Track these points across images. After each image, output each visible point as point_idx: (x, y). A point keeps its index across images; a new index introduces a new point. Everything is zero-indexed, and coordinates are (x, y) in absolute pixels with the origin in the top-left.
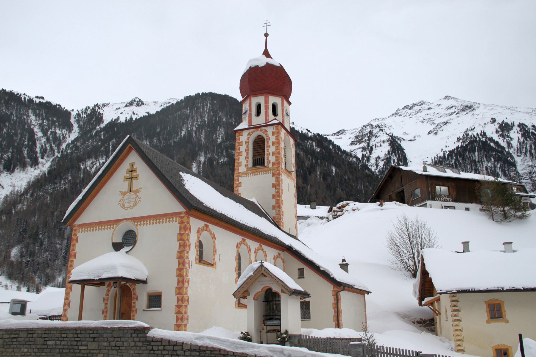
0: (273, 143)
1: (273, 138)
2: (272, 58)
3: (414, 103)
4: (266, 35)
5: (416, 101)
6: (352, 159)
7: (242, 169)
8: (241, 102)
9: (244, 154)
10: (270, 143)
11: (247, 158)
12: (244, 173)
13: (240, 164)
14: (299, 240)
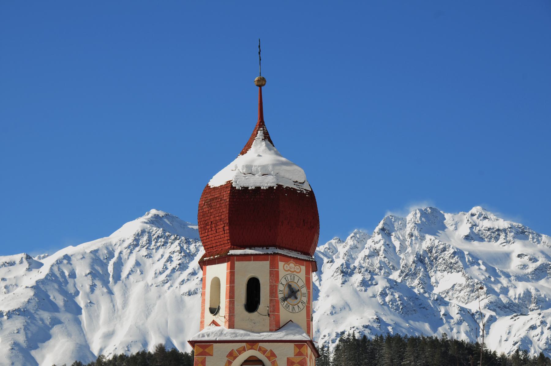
4: (261, 83)
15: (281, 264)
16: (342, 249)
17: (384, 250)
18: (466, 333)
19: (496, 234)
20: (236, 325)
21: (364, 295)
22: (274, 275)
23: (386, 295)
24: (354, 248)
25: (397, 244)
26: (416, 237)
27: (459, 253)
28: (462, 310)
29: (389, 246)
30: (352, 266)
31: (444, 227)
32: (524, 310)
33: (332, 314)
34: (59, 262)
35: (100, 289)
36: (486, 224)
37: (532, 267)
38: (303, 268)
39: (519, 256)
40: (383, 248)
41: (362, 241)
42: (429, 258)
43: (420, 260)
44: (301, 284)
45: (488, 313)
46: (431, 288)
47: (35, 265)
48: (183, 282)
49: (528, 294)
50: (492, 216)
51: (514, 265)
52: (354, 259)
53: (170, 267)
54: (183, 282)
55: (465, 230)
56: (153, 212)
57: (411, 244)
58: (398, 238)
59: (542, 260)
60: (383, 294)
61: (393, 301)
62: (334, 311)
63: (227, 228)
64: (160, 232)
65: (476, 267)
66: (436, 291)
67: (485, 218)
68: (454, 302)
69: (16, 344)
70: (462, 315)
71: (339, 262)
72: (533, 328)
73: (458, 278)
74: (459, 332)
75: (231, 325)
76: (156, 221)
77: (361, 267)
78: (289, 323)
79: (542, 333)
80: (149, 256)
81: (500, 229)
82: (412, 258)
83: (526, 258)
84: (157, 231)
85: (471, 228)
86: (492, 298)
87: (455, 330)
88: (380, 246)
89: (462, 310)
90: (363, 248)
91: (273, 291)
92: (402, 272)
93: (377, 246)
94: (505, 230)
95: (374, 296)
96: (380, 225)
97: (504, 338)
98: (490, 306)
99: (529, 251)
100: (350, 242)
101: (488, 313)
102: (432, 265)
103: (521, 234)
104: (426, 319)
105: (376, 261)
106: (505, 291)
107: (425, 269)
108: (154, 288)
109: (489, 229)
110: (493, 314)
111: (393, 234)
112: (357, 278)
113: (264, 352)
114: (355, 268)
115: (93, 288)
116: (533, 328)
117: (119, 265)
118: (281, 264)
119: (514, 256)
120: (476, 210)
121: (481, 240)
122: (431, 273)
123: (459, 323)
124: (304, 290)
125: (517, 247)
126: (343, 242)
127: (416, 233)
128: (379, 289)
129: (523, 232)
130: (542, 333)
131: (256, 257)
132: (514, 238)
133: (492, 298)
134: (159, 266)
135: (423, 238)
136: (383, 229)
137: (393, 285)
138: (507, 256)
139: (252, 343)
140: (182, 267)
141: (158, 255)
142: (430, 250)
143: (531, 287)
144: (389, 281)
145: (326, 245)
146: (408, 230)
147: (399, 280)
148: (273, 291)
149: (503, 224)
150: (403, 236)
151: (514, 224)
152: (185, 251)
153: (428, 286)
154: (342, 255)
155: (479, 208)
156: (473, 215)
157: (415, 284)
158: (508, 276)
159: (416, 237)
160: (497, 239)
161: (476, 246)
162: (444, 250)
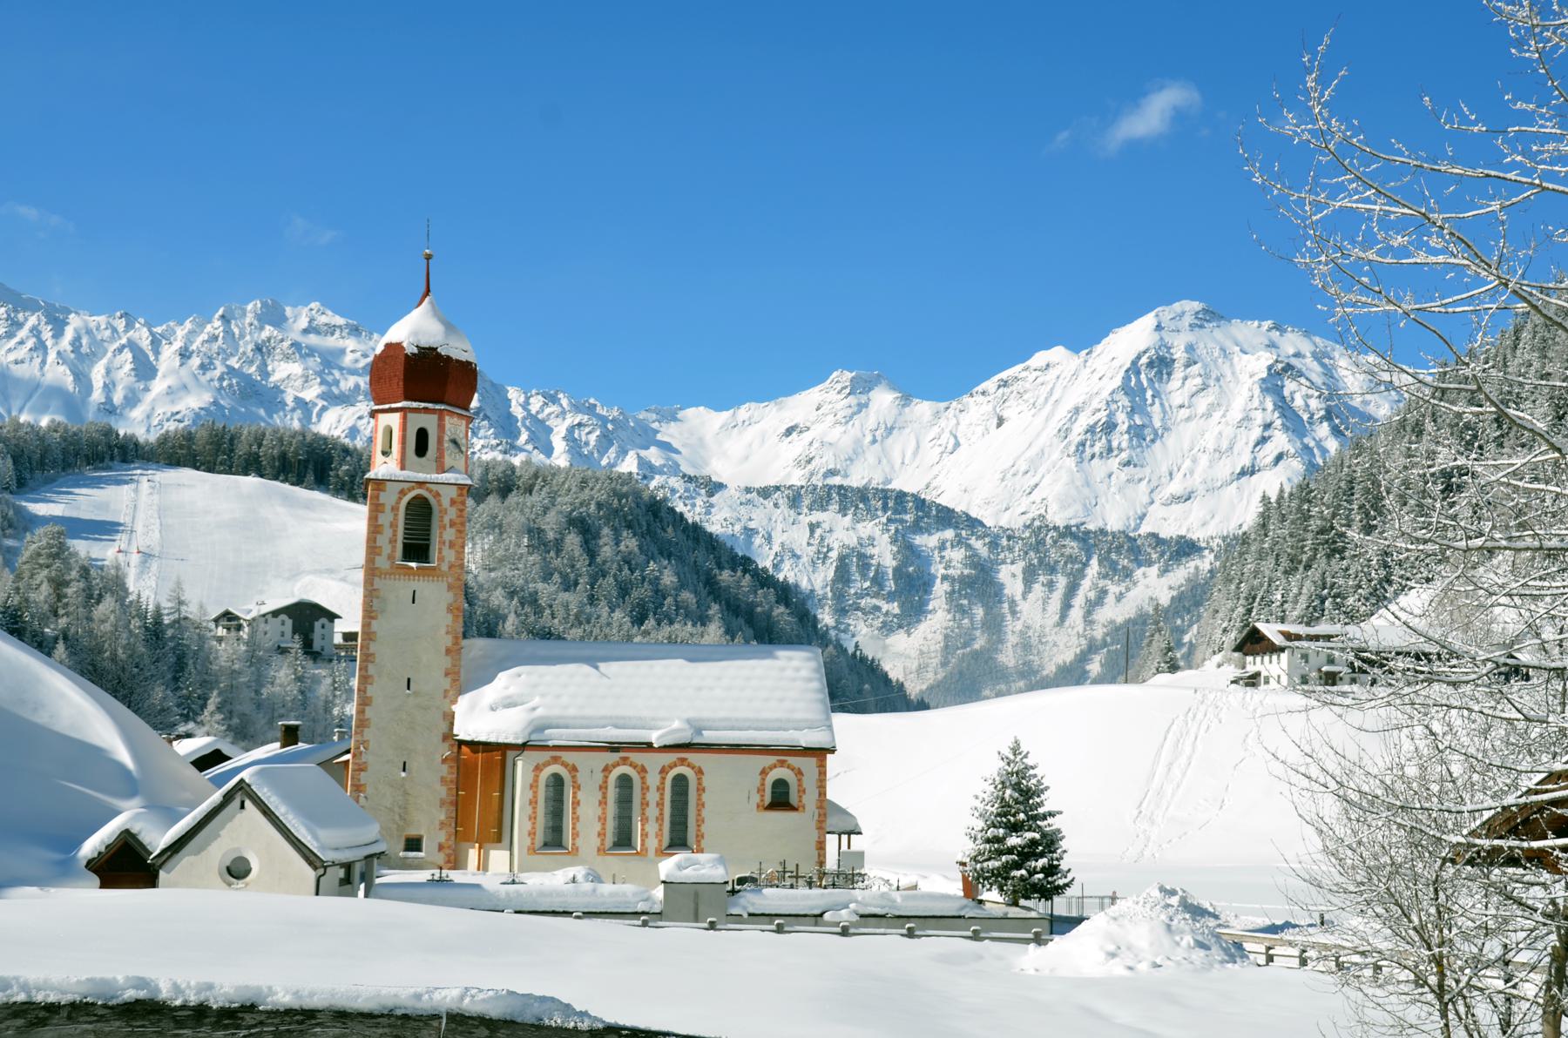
4: (428, 257)
10: (446, 520)
15: (447, 418)
16: (180, 332)
17: (223, 337)
18: (300, 420)
19: (331, 329)
20: (407, 467)
21: (203, 379)
22: (441, 427)
23: (224, 379)
24: (191, 332)
25: (236, 331)
26: (256, 327)
27: (295, 345)
28: (297, 399)
29: (228, 332)
30: (191, 349)
31: (285, 319)
32: (352, 400)
33: (167, 394)
36: (323, 319)
38: (464, 422)
39: (352, 351)
40: (221, 335)
41: (202, 326)
42: (267, 347)
43: (258, 349)
44: (462, 435)
45: (321, 403)
48: (10, 350)
50: (330, 313)
51: (348, 360)
52: (192, 343)
54: (10, 350)
55: (303, 323)
57: (250, 333)
58: (237, 326)
60: (221, 379)
61: (230, 386)
62: (170, 392)
63: (401, 383)
65: (312, 359)
66: (272, 379)
67: (323, 313)
68: (289, 390)
70: (296, 403)
71: (178, 345)
72: (360, 418)
73: (296, 368)
74: (292, 419)
75: (403, 468)
77: (199, 352)
78: (451, 469)
79: (369, 423)
81: (1109, 528)
82: (251, 347)
83: (359, 353)
85: (310, 322)
86: (324, 388)
87: (289, 417)
88: (220, 332)
89: (297, 399)
90: (202, 332)
91: (440, 441)
92: (240, 359)
93: (217, 332)
94: (340, 327)
95: (212, 380)
96: (221, 312)
97: (334, 426)
98: (322, 396)
99: (362, 347)
100: (188, 325)
101: (321, 403)
102: (269, 354)
103: (355, 331)
104: (261, 404)
105: (215, 347)
106: (337, 383)
107: (263, 357)
109: (326, 324)
110: (325, 403)
111: (233, 322)
112: (195, 362)
113: (430, 491)
114: (193, 352)
116: (360, 418)
118: (447, 418)
119: (348, 350)
122: (269, 362)
123: (293, 410)
125: (350, 343)
126: (182, 325)
127: (256, 323)
128: (217, 373)
129: (357, 330)
130: (369, 423)
131: (426, 410)
132: (349, 334)
133: (324, 388)
135: (262, 328)
136: (223, 317)
138: (343, 352)
139: (421, 484)
142: (269, 339)
144: (228, 366)
145: (164, 327)
146: (248, 320)
147: (237, 366)
148: (440, 441)
149: (340, 321)
150: (243, 324)
151: (350, 321)
152: (12, 319)
153: (266, 374)
154: (179, 338)
155: (318, 303)
156: (311, 310)
158: (341, 369)
159: (256, 327)
160: (332, 334)
161: (313, 339)
162: (282, 340)
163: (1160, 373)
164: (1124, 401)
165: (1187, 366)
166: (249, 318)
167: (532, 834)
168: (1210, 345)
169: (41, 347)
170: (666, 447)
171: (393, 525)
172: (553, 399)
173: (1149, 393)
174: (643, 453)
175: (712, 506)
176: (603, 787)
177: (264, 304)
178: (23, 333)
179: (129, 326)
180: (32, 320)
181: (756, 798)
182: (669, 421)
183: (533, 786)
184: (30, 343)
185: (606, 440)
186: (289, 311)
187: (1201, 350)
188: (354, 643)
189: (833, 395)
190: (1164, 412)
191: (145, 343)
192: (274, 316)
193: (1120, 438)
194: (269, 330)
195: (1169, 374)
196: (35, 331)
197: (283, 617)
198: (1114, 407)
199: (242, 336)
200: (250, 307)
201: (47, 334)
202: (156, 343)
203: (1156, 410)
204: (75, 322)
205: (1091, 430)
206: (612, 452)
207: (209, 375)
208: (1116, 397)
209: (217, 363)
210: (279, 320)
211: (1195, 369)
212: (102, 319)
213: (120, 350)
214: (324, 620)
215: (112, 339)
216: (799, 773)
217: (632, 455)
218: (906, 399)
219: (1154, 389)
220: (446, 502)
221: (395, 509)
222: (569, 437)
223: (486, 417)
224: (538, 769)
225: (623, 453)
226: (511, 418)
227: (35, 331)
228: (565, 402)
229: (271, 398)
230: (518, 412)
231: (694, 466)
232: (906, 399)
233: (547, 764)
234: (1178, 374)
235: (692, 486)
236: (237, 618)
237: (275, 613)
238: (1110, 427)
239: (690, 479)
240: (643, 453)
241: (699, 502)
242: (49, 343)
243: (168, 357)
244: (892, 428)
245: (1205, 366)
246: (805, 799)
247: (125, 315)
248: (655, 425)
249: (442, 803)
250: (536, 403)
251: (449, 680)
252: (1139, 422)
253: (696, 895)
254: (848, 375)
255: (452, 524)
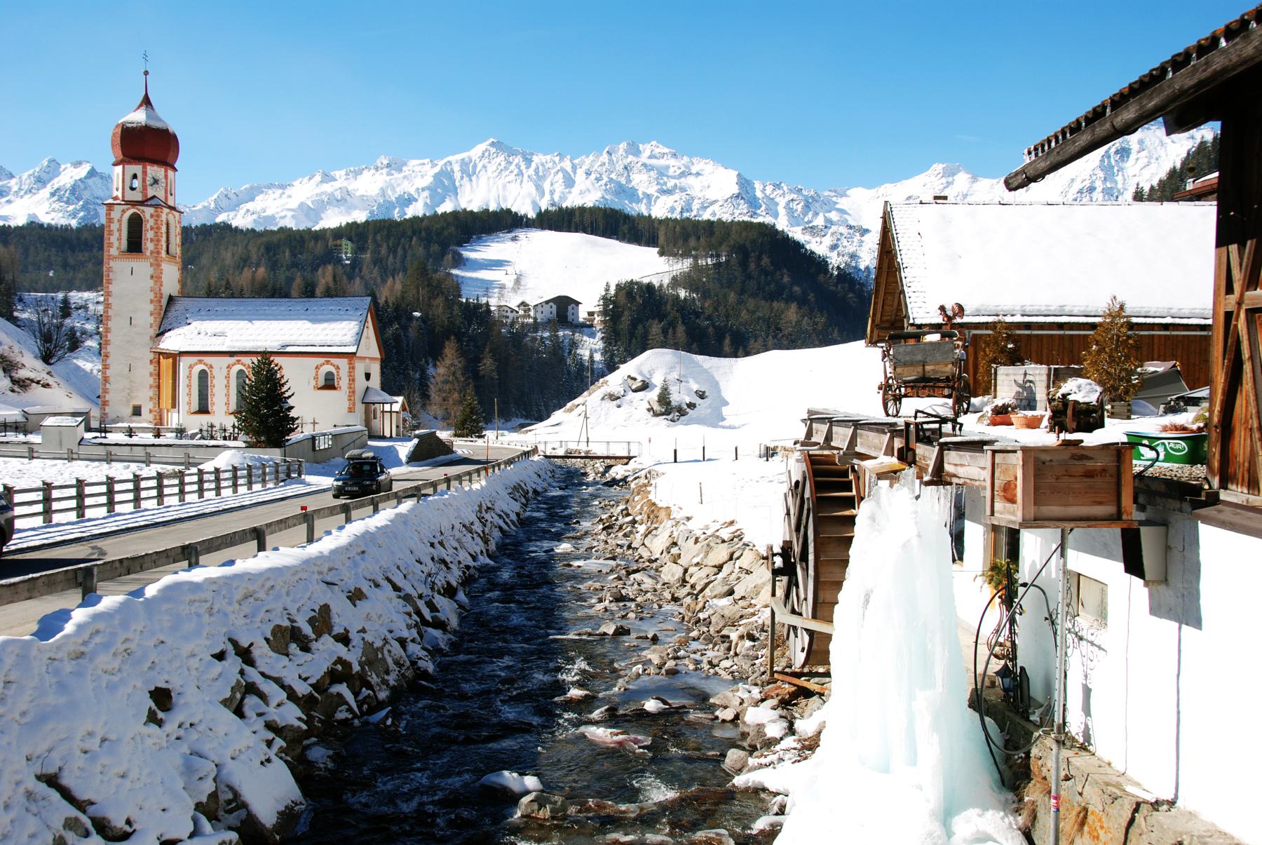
0: (152, 228)
1: (151, 222)
2: (195, 413)
3: (767, 785)
4: (146, 73)
5: (781, 790)
6: (703, 304)
7: (114, 251)
8: (279, 827)
9: (116, 234)
10: (148, 226)
11: (119, 239)
12: (115, 258)
13: (110, 245)
14: (146, 94)
21: (597, 185)
22: (145, 173)
25: (615, 159)
27: (644, 165)
28: (644, 193)
29: (611, 161)
34: (445, 164)
35: (466, 179)
36: (657, 151)
37: (678, 172)
41: (598, 157)
46: (631, 181)
47: (434, 165)
49: (676, 185)
51: (671, 172)
53: (500, 168)
55: (647, 153)
56: (492, 140)
59: (683, 169)
60: (606, 185)
64: (494, 150)
69: (426, 203)
71: (585, 167)
76: (493, 144)
80: (489, 162)
84: (493, 150)
86: (659, 187)
88: (606, 160)
98: (658, 191)
100: (591, 157)
103: (674, 155)
108: (492, 179)
115: (462, 178)
117: (475, 166)
120: (654, 143)
121: (656, 158)
124: (164, 180)
125: (672, 162)
128: (603, 182)
133: (659, 187)
134: (494, 168)
135: (627, 157)
137: (611, 180)
138: (668, 167)
140: (506, 168)
141: (493, 162)
143: (677, 181)
149: (666, 150)
153: (629, 180)
157: (623, 181)
158: (668, 176)
161: (653, 162)
163: (1122, 156)
164: (1101, 174)
165: (1139, 152)
166: (621, 152)
167: (189, 403)
168: (1153, 139)
169: (521, 174)
170: (842, 211)
171: (119, 230)
172: (777, 186)
173: (1116, 169)
174: (827, 215)
175: (862, 242)
176: (228, 377)
177: (628, 144)
178: (512, 167)
179: (561, 160)
180: (516, 161)
181: (313, 383)
182: (842, 196)
183: (189, 377)
184: (516, 171)
185: (807, 207)
186: (641, 147)
187: (1147, 143)
188: (1156, 341)
189: (933, 178)
190: (1125, 180)
191: (569, 169)
192: (634, 150)
193: (1098, 195)
194: (631, 158)
195: (1128, 157)
196: (518, 166)
197: (551, 304)
198: (1094, 178)
199: (617, 162)
200: (621, 146)
201: (523, 167)
202: (574, 168)
203: (1119, 179)
204: (536, 159)
205: (1080, 192)
206: (810, 215)
207: (600, 183)
208: (1096, 172)
209: (604, 176)
210: (637, 153)
211: (1144, 154)
212: (548, 157)
213: (557, 172)
214: (573, 305)
215: (553, 168)
216: (338, 368)
217: (821, 215)
218: (975, 179)
219: (1118, 166)
220: (148, 216)
221: (120, 221)
222: (787, 207)
223: (742, 198)
224: (191, 367)
225: (816, 214)
226: (755, 197)
227: (518, 166)
228: (785, 188)
229: (632, 194)
230: (759, 194)
231: (855, 221)
232: (975, 179)
233: (196, 364)
234: (1133, 156)
235: (851, 231)
236: (528, 305)
237: (547, 302)
238: (1091, 189)
239: (851, 227)
240: (827, 215)
241: (855, 240)
242: (524, 171)
243: (580, 177)
244: (967, 195)
245: (1149, 152)
246: (341, 383)
247: (559, 154)
248: (834, 199)
249: (151, 387)
250: (769, 190)
251: (152, 318)
252: (1109, 186)
253: (60, 433)
254: (941, 166)
255: (152, 228)
